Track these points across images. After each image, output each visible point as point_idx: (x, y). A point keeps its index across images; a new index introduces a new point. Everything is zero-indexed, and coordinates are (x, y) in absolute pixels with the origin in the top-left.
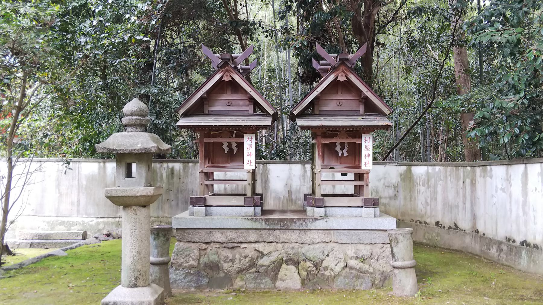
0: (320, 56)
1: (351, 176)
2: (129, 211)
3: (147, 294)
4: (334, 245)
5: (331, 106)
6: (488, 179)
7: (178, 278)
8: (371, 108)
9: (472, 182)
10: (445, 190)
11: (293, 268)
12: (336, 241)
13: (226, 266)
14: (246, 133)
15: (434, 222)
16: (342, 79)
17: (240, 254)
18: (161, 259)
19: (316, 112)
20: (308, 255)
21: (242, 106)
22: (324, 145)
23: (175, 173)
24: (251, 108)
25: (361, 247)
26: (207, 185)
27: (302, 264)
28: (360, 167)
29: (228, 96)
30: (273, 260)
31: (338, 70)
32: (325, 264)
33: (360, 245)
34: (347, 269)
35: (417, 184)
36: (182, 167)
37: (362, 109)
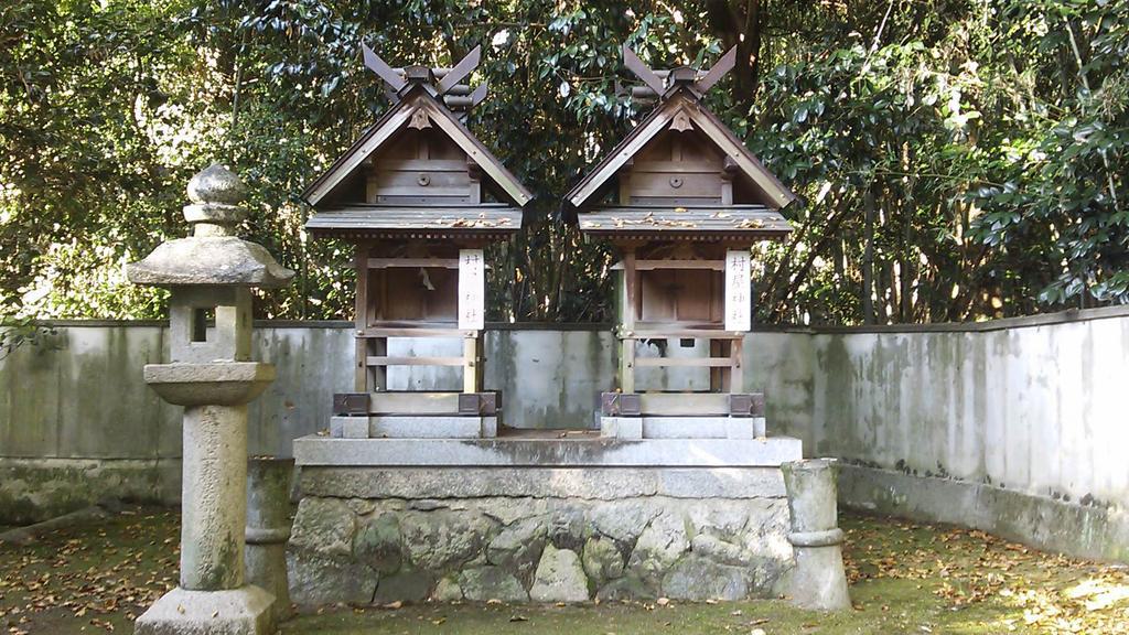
0: (632, 76)
1: (702, 338)
2: (200, 417)
3: (237, 606)
4: (661, 501)
5: (658, 187)
6: (1011, 358)
7: (306, 580)
8: (746, 193)
9: (976, 366)
10: (917, 388)
11: (568, 556)
12: (667, 492)
13: (416, 550)
14: (464, 248)
15: (892, 461)
16: (680, 125)
17: (449, 524)
18: (270, 531)
19: (624, 201)
20: (603, 524)
21: (454, 186)
22: (643, 273)
23: (293, 352)
24: (474, 191)
25: (725, 506)
26: (372, 368)
27: (592, 545)
28: (723, 327)
29: (421, 164)
30: (524, 537)
31: (672, 106)
32: (641, 544)
33: (722, 502)
34: (692, 556)
35: (856, 375)
36: (308, 339)
37: (727, 194)
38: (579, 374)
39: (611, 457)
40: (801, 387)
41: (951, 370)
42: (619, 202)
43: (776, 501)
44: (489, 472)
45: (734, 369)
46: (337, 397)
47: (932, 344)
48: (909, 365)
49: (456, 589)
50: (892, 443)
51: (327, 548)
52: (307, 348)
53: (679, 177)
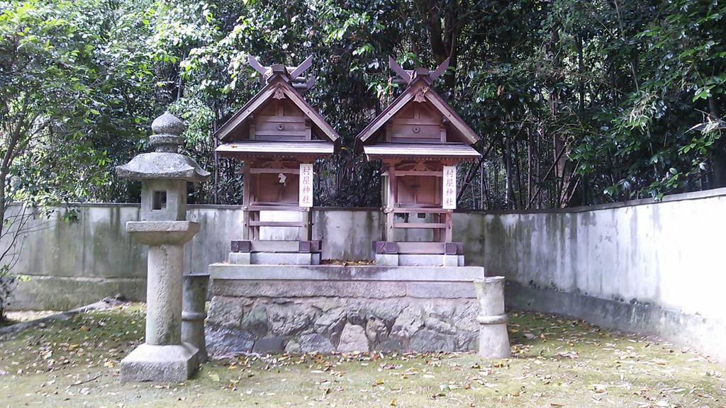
9: (572, 231)
12: (411, 294)
14: (302, 163)
18: (196, 314)
22: (398, 178)
23: (208, 221)
25: (440, 302)
29: (279, 119)
30: (334, 319)
32: (398, 323)
34: (425, 329)
37: (443, 137)
38: (361, 235)
39: (383, 276)
40: (478, 242)
41: (558, 233)
42: (385, 140)
43: (470, 300)
44: (316, 284)
45: (447, 229)
46: (233, 242)
47: (548, 220)
48: (536, 230)
49: (297, 346)
50: (526, 271)
51: (227, 323)
52: (216, 219)
53: (418, 127)
